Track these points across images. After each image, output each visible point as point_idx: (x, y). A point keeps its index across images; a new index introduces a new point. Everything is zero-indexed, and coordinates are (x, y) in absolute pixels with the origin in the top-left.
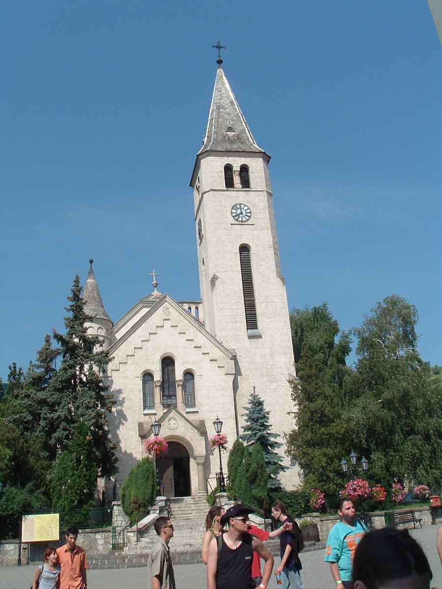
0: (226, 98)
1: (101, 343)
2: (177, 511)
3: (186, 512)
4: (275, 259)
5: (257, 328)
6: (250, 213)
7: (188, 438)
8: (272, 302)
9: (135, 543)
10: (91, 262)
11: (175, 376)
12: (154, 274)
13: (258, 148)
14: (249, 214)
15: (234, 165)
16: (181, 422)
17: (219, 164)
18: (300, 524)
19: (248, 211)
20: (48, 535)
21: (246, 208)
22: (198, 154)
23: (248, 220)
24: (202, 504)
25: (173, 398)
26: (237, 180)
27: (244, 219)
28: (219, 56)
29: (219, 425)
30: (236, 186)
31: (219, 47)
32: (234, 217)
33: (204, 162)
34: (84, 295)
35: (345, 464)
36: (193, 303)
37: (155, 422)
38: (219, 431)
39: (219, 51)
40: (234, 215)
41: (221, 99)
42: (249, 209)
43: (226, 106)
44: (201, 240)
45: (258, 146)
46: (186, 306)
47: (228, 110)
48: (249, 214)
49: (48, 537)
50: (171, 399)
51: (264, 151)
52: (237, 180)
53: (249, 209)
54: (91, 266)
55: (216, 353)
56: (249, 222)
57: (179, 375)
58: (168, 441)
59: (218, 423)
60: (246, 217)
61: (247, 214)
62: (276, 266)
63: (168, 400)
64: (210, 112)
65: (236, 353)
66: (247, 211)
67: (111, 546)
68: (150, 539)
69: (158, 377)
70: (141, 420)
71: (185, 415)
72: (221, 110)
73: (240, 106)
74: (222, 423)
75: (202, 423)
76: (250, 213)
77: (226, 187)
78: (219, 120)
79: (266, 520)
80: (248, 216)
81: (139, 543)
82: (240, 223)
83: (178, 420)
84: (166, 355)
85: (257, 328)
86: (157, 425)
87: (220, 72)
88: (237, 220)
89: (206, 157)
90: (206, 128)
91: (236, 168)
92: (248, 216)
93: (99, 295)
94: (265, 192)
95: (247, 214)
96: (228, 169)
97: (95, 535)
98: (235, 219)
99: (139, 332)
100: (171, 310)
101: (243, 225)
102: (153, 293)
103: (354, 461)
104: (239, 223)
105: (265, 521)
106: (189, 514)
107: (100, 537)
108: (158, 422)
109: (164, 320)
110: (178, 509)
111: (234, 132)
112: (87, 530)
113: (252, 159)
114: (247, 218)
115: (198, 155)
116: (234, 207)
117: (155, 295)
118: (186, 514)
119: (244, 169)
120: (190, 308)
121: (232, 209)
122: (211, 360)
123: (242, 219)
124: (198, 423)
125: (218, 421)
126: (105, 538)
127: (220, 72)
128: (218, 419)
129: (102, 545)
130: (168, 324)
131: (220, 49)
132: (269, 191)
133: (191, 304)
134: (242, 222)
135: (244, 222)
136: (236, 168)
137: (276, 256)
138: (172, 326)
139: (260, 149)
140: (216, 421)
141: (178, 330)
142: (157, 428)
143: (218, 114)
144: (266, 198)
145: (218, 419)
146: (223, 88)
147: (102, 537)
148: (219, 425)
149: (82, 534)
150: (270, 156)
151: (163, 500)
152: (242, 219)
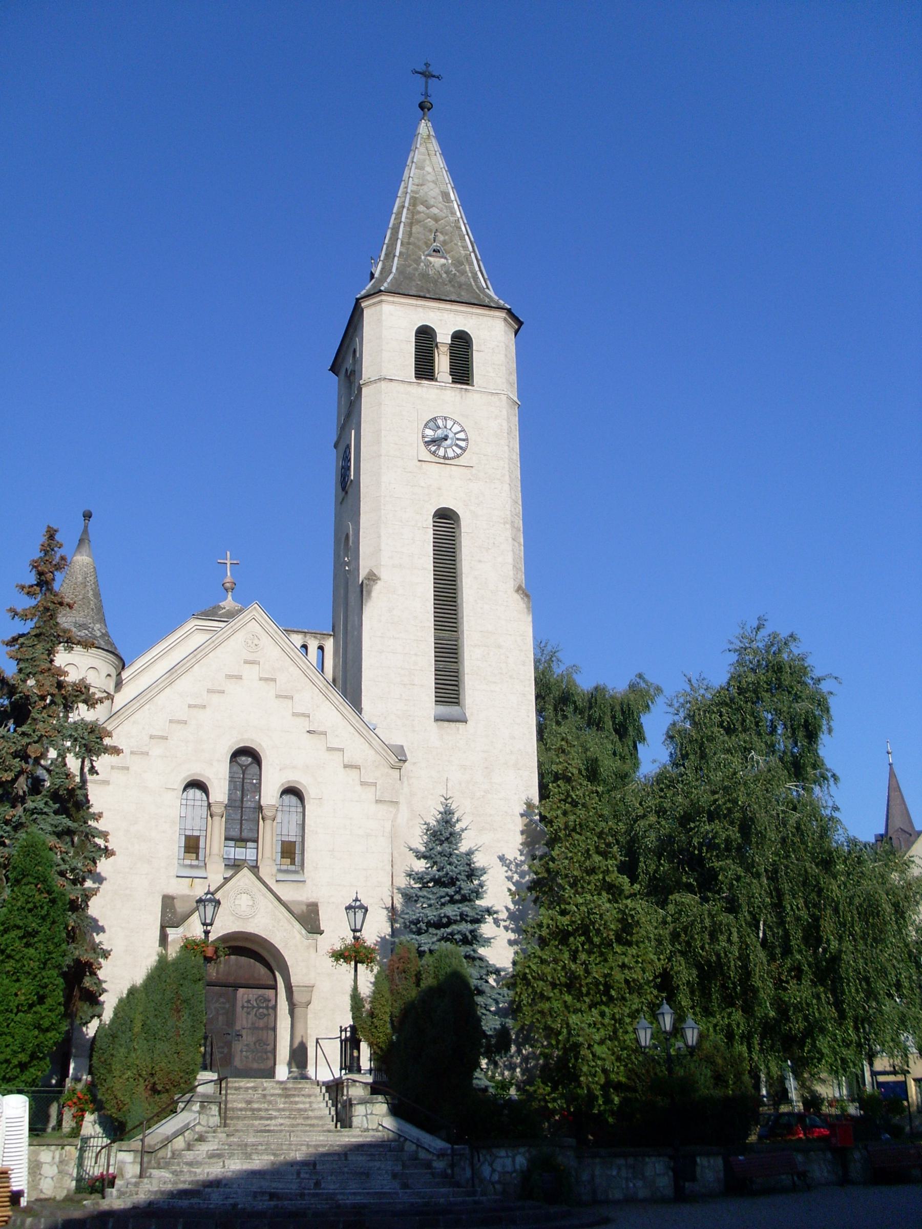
0: (432, 185)
1: (91, 702)
2: (241, 1110)
3: (263, 1114)
4: (513, 550)
5: (458, 703)
6: (465, 440)
7: (277, 940)
8: (500, 647)
9: (134, 1180)
10: (88, 516)
12: (228, 562)
13: (496, 298)
14: (462, 444)
16: (266, 903)
19: (461, 435)
21: (456, 428)
22: (358, 296)
23: (458, 456)
24: (303, 1099)
25: (250, 844)
26: (442, 363)
27: (450, 454)
28: (426, 95)
29: (360, 914)
30: (439, 377)
31: (427, 75)
33: (369, 315)
34: (62, 584)
35: (645, 1029)
36: (314, 634)
37: (207, 894)
38: (358, 927)
39: (427, 82)
41: (422, 185)
42: (463, 431)
43: (432, 202)
44: (347, 493)
45: (496, 294)
46: (298, 640)
47: (434, 210)
48: (462, 444)
51: (509, 307)
52: (442, 363)
53: (463, 431)
56: (462, 461)
57: (270, 794)
58: (228, 945)
59: (356, 908)
60: (454, 448)
61: (458, 442)
62: (514, 566)
64: (395, 210)
65: (405, 756)
66: (457, 436)
67: (74, 1183)
68: (173, 1173)
69: (220, 792)
70: (171, 891)
71: (274, 887)
72: (421, 208)
73: (463, 204)
74: (366, 910)
75: (313, 908)
76: (465, 440)
77: (416, 377)
78: (414, 230)
79: (456, 1147)
80: (461, 448)
81: (146, 1180)
85: (458, 703)
86: (210, 900)
87: (424, 128)
88: (434, 453)
91: (444, 337)
92: (461, 448)
93: (97, 595)
94: (504, 398)
95: (458, 442)
96: (425, 336)
99: (184, 684)
100: (266, 641)
102: (222, 604)
103: (668, 1022)
104: (442, 461)
105: (452, 1149)
106: (270, 1118)
108: (213, 894)
109: (246, 662)
110: (243, 1105)
114: (459, 451)
115: (358, 300)
116: (432, 423)
117: (227, 608)
118: (261, 1118)
120: (305, 647)
121: (426, 426)
122: (346, 766)
123: (446, 452)
124: (304, 908)
125: (358, 903)
126: (61, 1162)
127: (424, 128)
128: (356, 900)
129: (52, 1178)
130: (251, 673)
131: (430, 81)
132: (512, 396)
133: (308, 636)
134: (445, 458)
135: (448, 459)
136: (444, 337)
137: (516, 544)
139: (502, 302)
140: (353, 904)
142: (210, 908)
143: (413, 213)
144: (504, 412)
145: (356, 900)
146: (428, 162)
148: (360, 914)
150: (522, 320)
151: (212, 1081)
152: (446, 452)
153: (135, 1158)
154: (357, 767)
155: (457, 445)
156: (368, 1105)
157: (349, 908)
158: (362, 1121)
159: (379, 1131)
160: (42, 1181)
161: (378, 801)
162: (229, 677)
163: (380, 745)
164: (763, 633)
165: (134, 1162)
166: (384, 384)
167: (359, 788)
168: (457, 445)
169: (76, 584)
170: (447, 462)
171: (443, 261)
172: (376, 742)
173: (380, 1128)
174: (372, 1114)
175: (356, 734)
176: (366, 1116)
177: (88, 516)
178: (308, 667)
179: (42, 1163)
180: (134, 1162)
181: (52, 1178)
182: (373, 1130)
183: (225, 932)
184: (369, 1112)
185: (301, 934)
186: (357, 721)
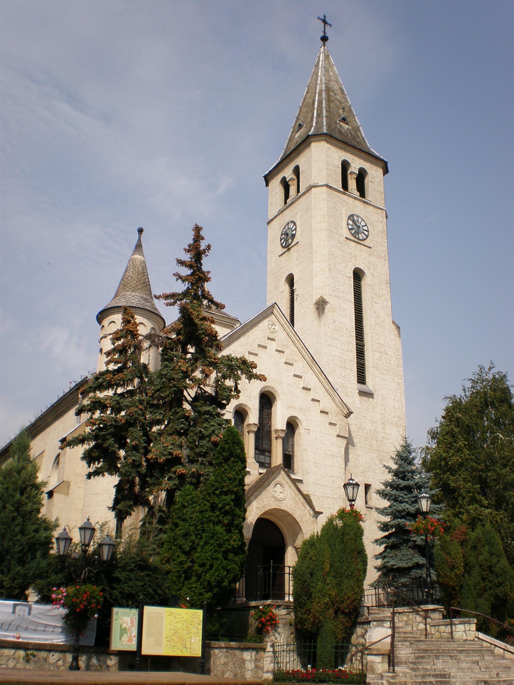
7: (297, 516)
8: (387, 354)
10: (140, 231)
11: (271, 423)
15: (352, 165)
17: (336, 157)
18: (373, 662)
20: (185, 647)
21: (363, 223)
23: (364, 240)
31: (325, 22)
32: (350, 229)
40: (350, 227)
42: (366, 225)
49: (184, 650)
50: (264, 455)
52: (352, 184)
53: (366, 225)
54: (140, 238)
55: (327, 403)
56: (365, 243)
63: (261, 456)
82: (357, 240)
83: (286, 486)
84: (266, 390)
89: (319, 141)
90: (314, 109)
97: (242, 655)
98: (351, 233)
100: (278, 327)
101: (361, 244)
104: (357, 240)
107: (249, 658)
111: (348, 125)
112: (232, 643)
113: (372, 166)
119: (361, 176)
126: (256, 660)
129: (252, 671)
130: (272, 346)
138: (276, 351)
141: (283, 358)
147: (251, 657)
148: (88, 533)
149: (225, 650)
153: (383, 659)
154: (326, 413)
155: (364, 233)
156: (466, 624)
157: (81, 529)
158: (463, 635)
159: (476, 641)
160: (246, 673)
161: (338, 436)
162: (260, 346)
163: (339, 401)
164: (493, 371)
165: (383, 662)
166: (313, 189)
167: (328, 426)
168: (364, 233)
169: (138, 272)
170: (359, 241)
171: (347, 126)
172: (337, 399)
173: (476, 639)
174: (469, 630)
175: (326, 392)
176: (465, 632)
177: (140, 231)
178: (302, 348)
179: (245, 660)
180: (383, 662)
181: (252, 671)
182: (470, 640)
183: (270, 508)
184: (467, 629)
185: (310, 513)
186: (328, 385)
